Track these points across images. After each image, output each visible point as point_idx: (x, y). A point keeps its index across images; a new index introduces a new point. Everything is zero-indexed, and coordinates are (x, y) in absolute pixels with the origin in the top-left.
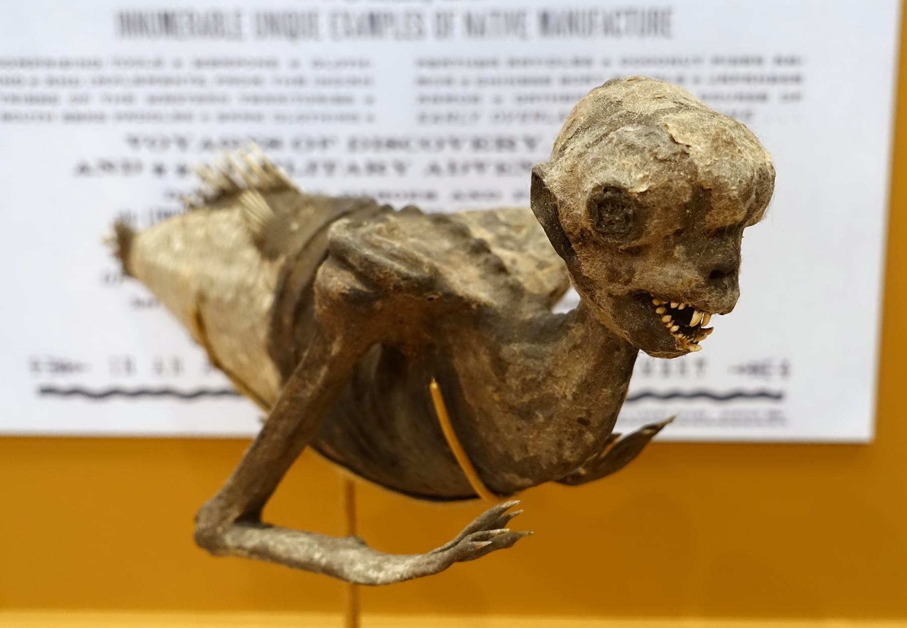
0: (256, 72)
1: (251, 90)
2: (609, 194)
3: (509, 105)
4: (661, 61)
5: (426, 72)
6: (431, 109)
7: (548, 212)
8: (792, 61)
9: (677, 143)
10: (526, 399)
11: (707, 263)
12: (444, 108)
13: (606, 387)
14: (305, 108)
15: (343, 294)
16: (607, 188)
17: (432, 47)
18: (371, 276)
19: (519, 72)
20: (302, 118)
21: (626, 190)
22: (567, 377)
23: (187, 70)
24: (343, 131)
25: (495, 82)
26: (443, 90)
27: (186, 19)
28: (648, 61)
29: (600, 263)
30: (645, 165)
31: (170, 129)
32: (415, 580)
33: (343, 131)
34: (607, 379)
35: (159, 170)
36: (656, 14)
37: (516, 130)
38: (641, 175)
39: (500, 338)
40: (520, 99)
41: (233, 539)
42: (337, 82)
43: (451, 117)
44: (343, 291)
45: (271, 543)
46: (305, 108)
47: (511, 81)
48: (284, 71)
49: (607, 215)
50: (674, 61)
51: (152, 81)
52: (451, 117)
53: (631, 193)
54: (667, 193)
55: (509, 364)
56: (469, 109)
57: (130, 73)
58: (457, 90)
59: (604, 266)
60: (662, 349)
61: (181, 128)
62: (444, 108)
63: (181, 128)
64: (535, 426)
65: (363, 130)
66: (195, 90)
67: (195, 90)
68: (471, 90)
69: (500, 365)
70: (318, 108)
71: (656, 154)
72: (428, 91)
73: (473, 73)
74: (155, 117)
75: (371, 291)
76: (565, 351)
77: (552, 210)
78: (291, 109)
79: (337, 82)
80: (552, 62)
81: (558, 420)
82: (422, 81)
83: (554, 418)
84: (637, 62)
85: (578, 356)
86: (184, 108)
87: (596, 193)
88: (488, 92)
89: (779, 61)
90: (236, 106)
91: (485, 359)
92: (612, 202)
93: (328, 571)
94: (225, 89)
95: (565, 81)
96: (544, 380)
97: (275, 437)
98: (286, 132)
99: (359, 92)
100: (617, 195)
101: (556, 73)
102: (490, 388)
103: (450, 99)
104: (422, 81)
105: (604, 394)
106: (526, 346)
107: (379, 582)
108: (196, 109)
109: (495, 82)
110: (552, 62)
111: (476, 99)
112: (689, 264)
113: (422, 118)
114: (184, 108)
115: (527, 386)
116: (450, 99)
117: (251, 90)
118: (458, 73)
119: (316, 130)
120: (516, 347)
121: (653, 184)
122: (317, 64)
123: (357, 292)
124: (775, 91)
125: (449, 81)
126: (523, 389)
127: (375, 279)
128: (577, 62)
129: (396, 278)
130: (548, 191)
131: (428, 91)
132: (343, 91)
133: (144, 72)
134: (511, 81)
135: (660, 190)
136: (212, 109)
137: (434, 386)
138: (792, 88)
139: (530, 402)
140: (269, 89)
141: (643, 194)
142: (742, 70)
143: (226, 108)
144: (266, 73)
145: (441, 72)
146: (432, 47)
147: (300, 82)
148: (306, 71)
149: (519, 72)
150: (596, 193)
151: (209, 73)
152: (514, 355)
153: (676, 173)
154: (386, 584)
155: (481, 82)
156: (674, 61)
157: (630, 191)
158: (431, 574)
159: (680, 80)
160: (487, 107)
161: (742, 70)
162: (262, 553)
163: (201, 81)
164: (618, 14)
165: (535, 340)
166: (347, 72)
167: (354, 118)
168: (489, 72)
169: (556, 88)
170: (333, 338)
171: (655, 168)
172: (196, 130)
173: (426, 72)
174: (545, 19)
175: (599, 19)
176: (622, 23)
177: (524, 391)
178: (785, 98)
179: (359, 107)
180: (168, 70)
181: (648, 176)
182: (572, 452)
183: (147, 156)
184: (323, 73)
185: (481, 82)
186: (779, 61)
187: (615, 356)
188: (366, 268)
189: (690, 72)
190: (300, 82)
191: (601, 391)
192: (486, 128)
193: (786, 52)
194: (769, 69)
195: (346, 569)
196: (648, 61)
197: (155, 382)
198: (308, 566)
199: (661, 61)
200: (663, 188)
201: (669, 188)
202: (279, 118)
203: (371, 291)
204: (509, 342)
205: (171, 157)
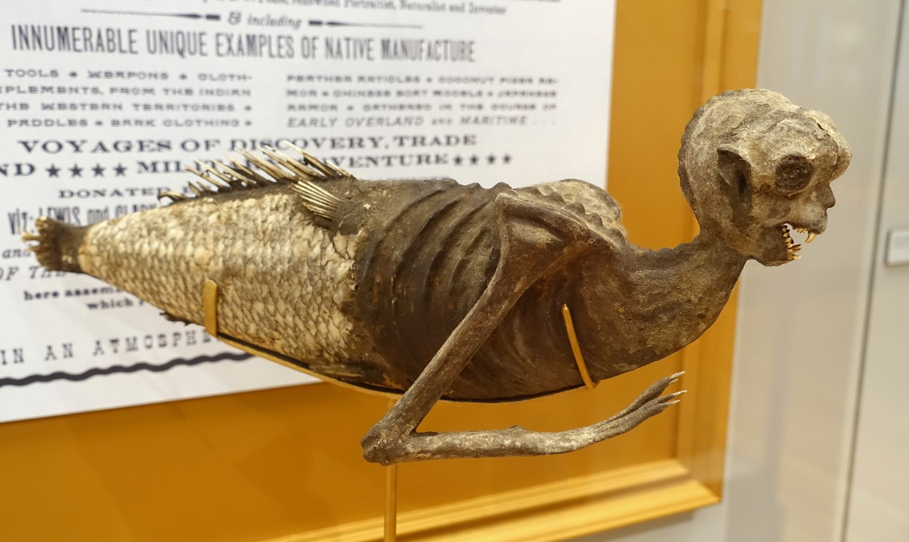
0: (148, 83)
1: (143, 99)
2: (792, 161)
3: (359, 113)
4: (466, 80)
5: (294, 85)
6: (298, 115)
7: (730, 176)
8: (550, 81)
9: (822, 129)
10: (651, 308)
11: (827, 202)
12: (308, 115)
13: (722, 291)
14: (191, 115)
15: (547, 244)
16: (792, 157)
17: (299, 65)
18: (563, 230)
19: (366, 86)
20: (189, 123)
21: (804, 158)
22: (690, 288)
23: (83, 80)
24: (225, 134)
25: (348, 94)
26: (308, 100)
27: (79, 34)
28: (458, 80)
29: (766, 206)
30: (811, 142)
31: (65, 134)
32: (607, 440)
33: (225, 134)
34: (724, 285)
35: (53, 171)
36: (463, 43)
37: (364, 132)
38: (810, 149)
39: (627, 268)
40: (367, 107)
41: (414, 447)
42: (220, 92)
43: (314, 122)
44: (547, 242)
45: (457, 442)
46: (191, 115)
47: (361, 93)
48: (174, 82)
49: (785, 175)
50: (475, 80)
51: (46, 89)
52: (314, 122)
53: (808, 160)
54: (826, 159)
55: (636, 285)
56: (328, 115)
57: (25, 83)
58: (319, 100)
59: (768, 208)
60: (779, 260)
61: (76, 133)
62: (308, 115)
63: (76, 133)
64: (659, 325)
65: (243, 133)
66: (91, 98)
67: (91, 98)
68: (330, 100)
69: (628, 287)
70: (202, 115)
71: (816, 136)
72: (297, 101)
73: (331, 87)
74: (48, 123)
75: (562, 241)
76: (688, 271)
77: (732, 174)
78: (180, 115)
79: (220, 92)
80: (391, 79)
81: (680, 318)
82: (292, 93)
83: (677, 317)
84: (451, 80)
85: (700, 273)
86: (78, 115)
87: (784, 161)
88: (343, 102)
89: (542, 81)
90: (127, 112)
91: (613, 284)
92: (792, 167)
93: (523, 451)
94: (117, 98)
95: (400, 93)
96: (669, 292)
97: (456, 361)
98: (175, 136)
99: (239, 102)
100: (797, 161)
101: (394, 87)
102: (617, 304)
103: (313, 107)
104: (292, 93)
105: (719, 296)
106: (648, 272)
107: (585, 445)
108: (91, 116)
109: (348, 94)
110: (391, 79)
111: (334, 107)
112: (818, 203)
113: (291, 122)
114: (78, 115)
115: (652, 299)
116: (313, 107)
117: (143, 99)
118: (320, 86)
119: (201, 134)
120: (641, 273)
121: (818, 154)
122: (202, 77)
123: (555, 242)
124: (540, 102)
125: (313, 93)
126: (649, 301)
127: (566, 231)
128: (408, 79)
129: (579, 230)
130: (744, 161)
131: (297, 101)
132: (225, 100)
133: (38, 82)
134: (361, 93)
135: (822, 157)
136: (106, 116)
137: (566, 308)
138: (550, 100)
139: (655, 309)
140: (160, 98)
141: (813, 160)
142: (519, 87)
143: (119, 115)
144: (158, 85)
145: (307, 86)
146: (299, 65)
147: (189, 92)
148: (192, 82)
149: (366, 86)
150: (784, 161)
151: (104, 84)
152: (641, 278)
153: (830, 147)
154: (580, 448)
155: (337, 94)
156: (475, 80)
157: (807, 158)
158: (624, 432)
159: (480, 94)
160: (342, 114)
161: (519, 87)
162: (449, 452)
163: (95, 90)
164: (437, 42)
165: (653, 267)
166: (229, 85)
167: (236, 123)
168: (344, 86)
169: (394, 100)
170: (518, 279)
171: (818, 144)
172: (91, 135)
173: (294, 85)
174: (385, 45)
175: (425, 46)
176: (440, 50)
177: (650, 303)
178: (546, 107)
179: (239, 114)
180: (64, 80)
181: (814, 149)
182: (687, 339)
183: (42, 160)
184: (208, 84)
185: (337, 94)
186: (542, 81)
187: (733, 269)
188: (560, 224)
189: (486, 88)
190: (189, 92)
191: (719, 294)
192: (341, 131)
193: (546, 76)
194: (535, 87)
195: (540, 446)
196: (458, 80)
197: (45, 369)
198: (498, 452)
199: (466, 80)
200: (823, 156)
201: (828, 156)
202: (167, 123)
203: (562, 241)
204: (634, 270)
205: (65, 160)
